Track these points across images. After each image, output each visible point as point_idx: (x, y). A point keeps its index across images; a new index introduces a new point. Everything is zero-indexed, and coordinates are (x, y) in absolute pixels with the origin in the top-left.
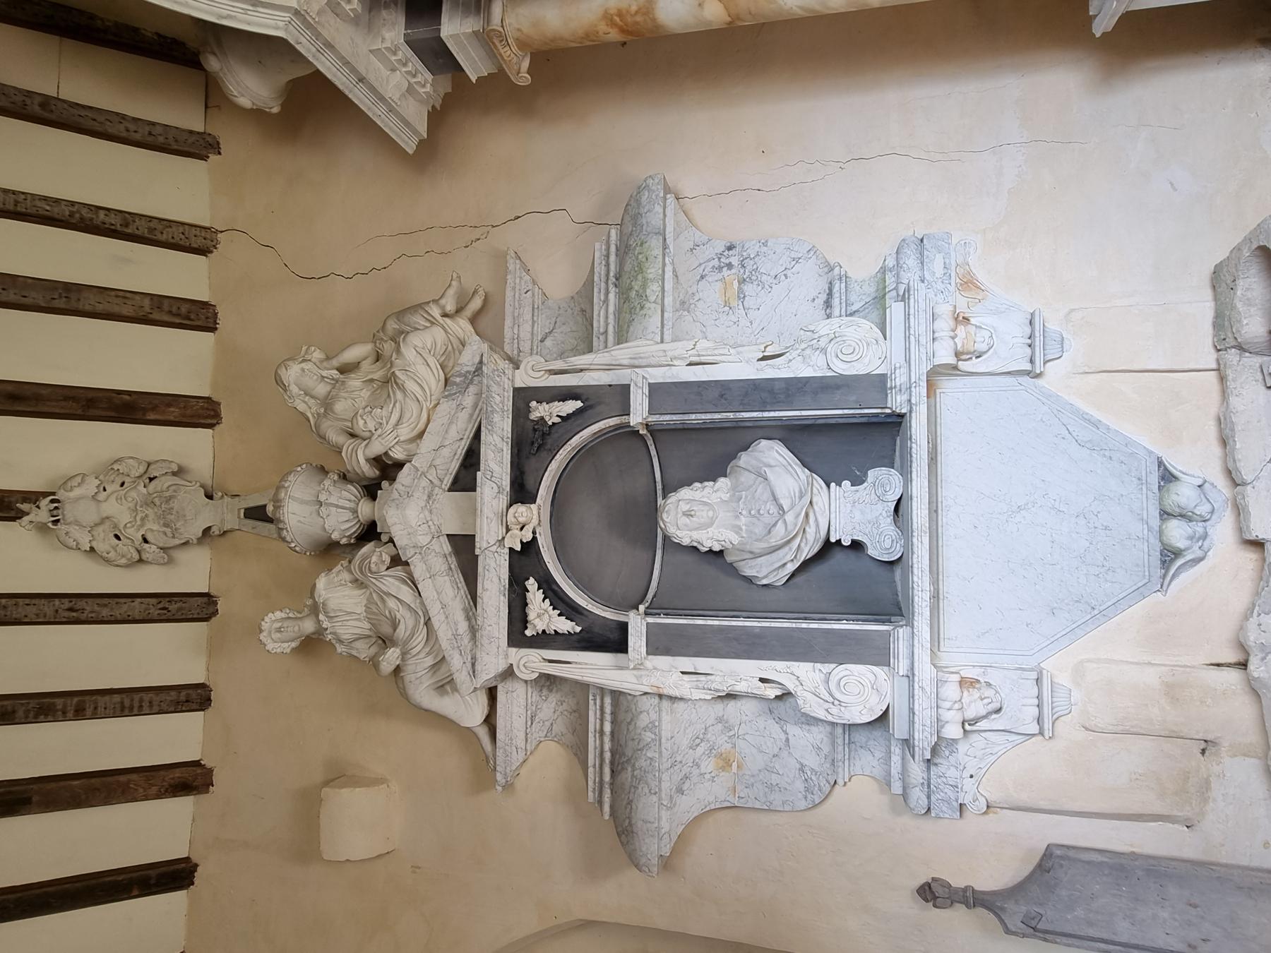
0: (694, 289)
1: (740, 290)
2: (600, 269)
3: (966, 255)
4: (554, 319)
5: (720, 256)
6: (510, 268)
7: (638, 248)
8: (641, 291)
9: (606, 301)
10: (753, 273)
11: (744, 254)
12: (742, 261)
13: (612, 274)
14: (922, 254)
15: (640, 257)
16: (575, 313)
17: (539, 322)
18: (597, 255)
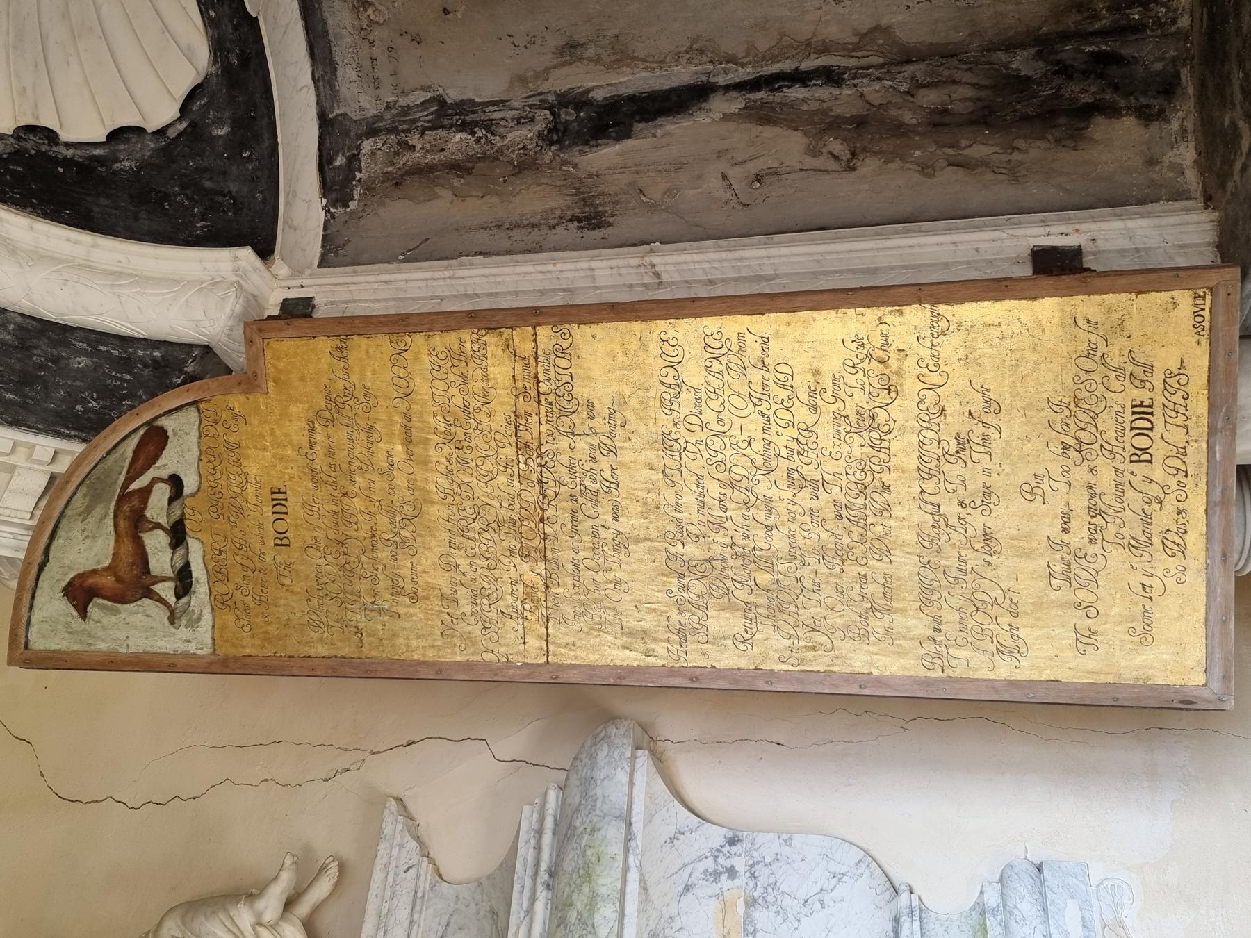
0: (672, 910)
1: (748, 919)
2: (525, 852)
3: (1116, 908)
4: (446, 918)
5: (717, 854)
6: (385, 833)
7: (586, 837)
8: (585, 915)
9: (530, 912)
10: (770, 889)
11: (755, 854)
12: (752, 866)
13: (543, 867)
14: (1042, 894)
15: (589, 852)
16: (482, 913)
17: (422, 924)
18: (524, 826)
